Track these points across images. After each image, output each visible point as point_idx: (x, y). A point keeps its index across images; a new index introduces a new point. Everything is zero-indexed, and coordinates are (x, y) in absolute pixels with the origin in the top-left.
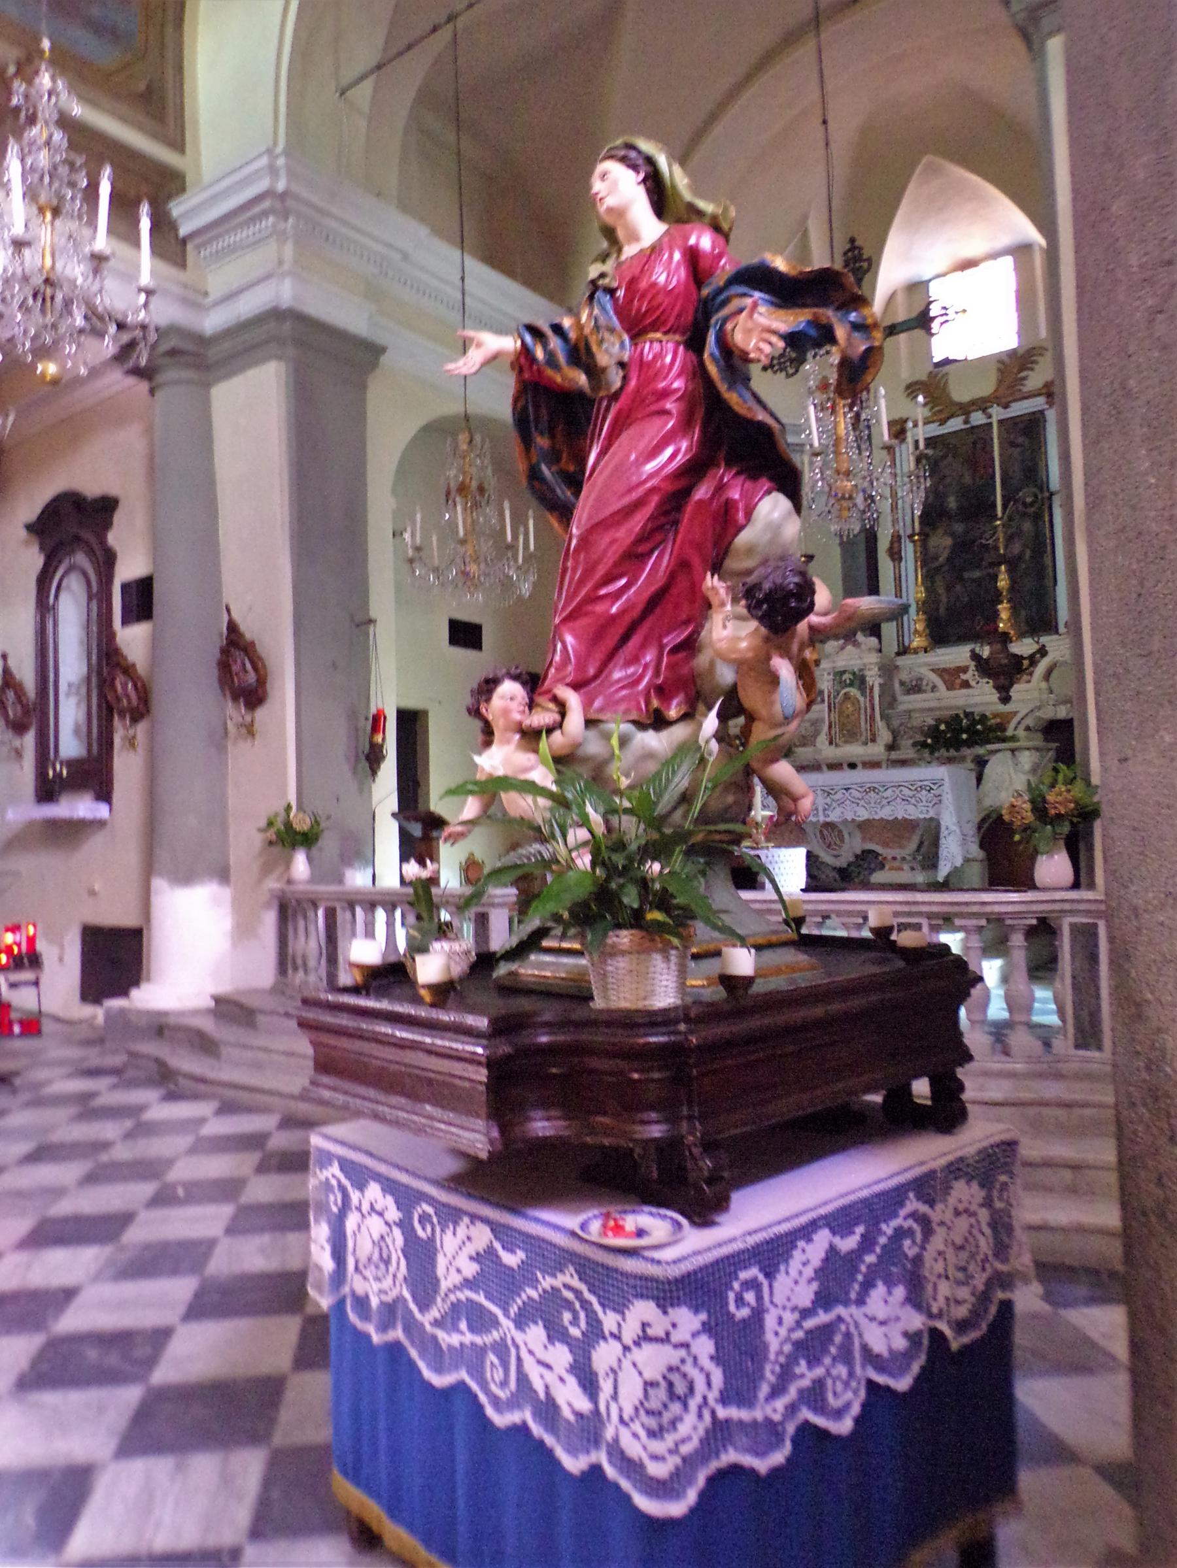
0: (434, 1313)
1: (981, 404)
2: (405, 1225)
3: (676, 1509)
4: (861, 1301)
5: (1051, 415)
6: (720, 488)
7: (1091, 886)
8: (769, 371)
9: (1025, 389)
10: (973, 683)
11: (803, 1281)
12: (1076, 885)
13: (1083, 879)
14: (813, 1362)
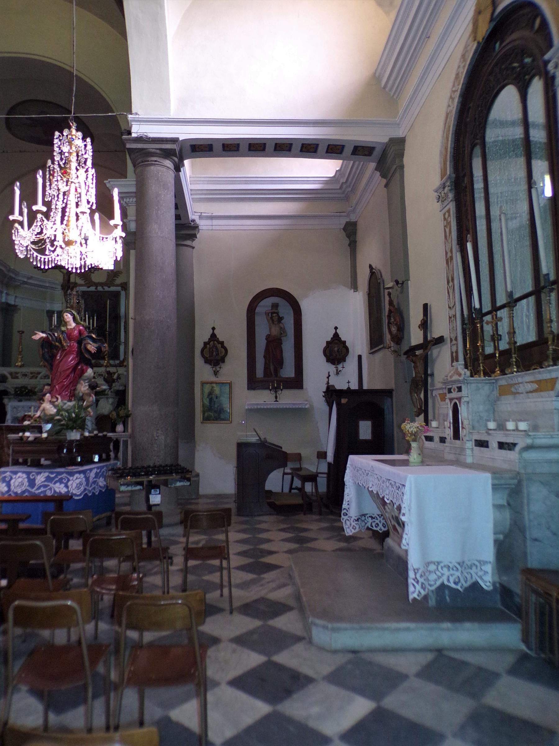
0: (35, 489)
1: (102, 285)
2: (28, 478)
3: (81, 497)
4: (55, 483)
5: (123, 293)
6: (82, 367)
7: (128, 431)
8: (36, 269)
9: (115, 283)
10: (96, 377)
11: (43, 477)
12: (124, 432)
13: (126, 430)
14: (94, 484)
